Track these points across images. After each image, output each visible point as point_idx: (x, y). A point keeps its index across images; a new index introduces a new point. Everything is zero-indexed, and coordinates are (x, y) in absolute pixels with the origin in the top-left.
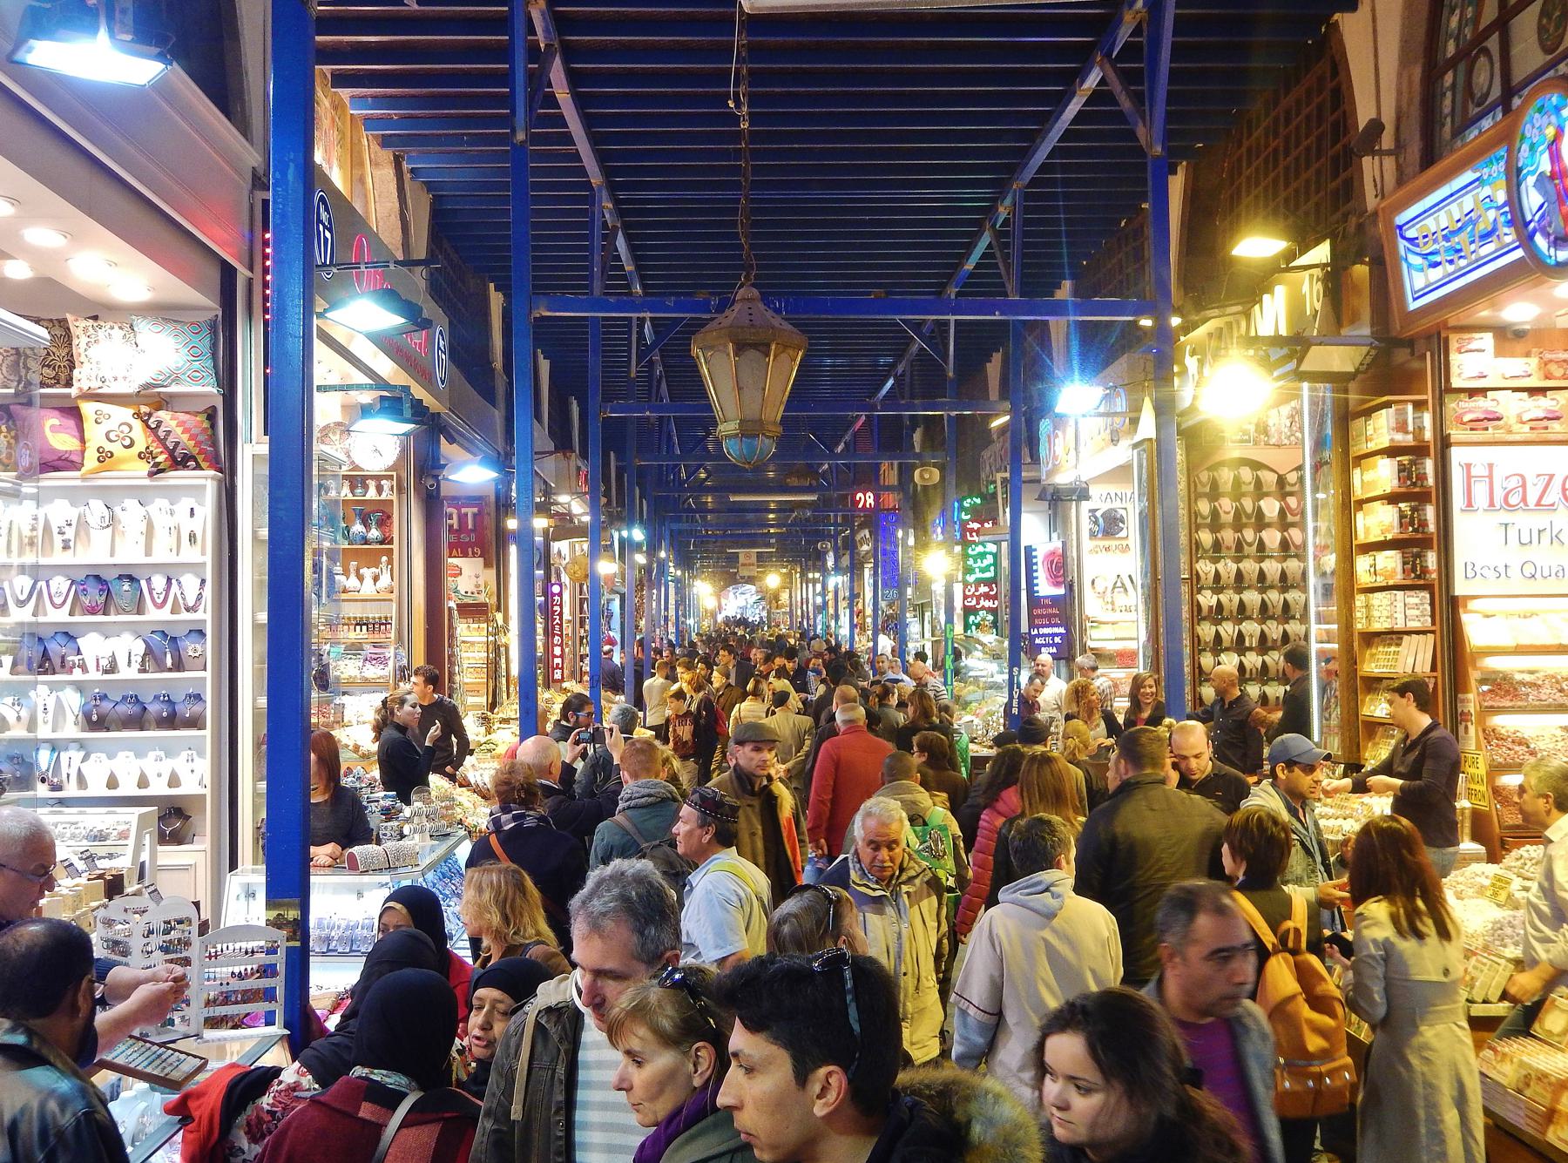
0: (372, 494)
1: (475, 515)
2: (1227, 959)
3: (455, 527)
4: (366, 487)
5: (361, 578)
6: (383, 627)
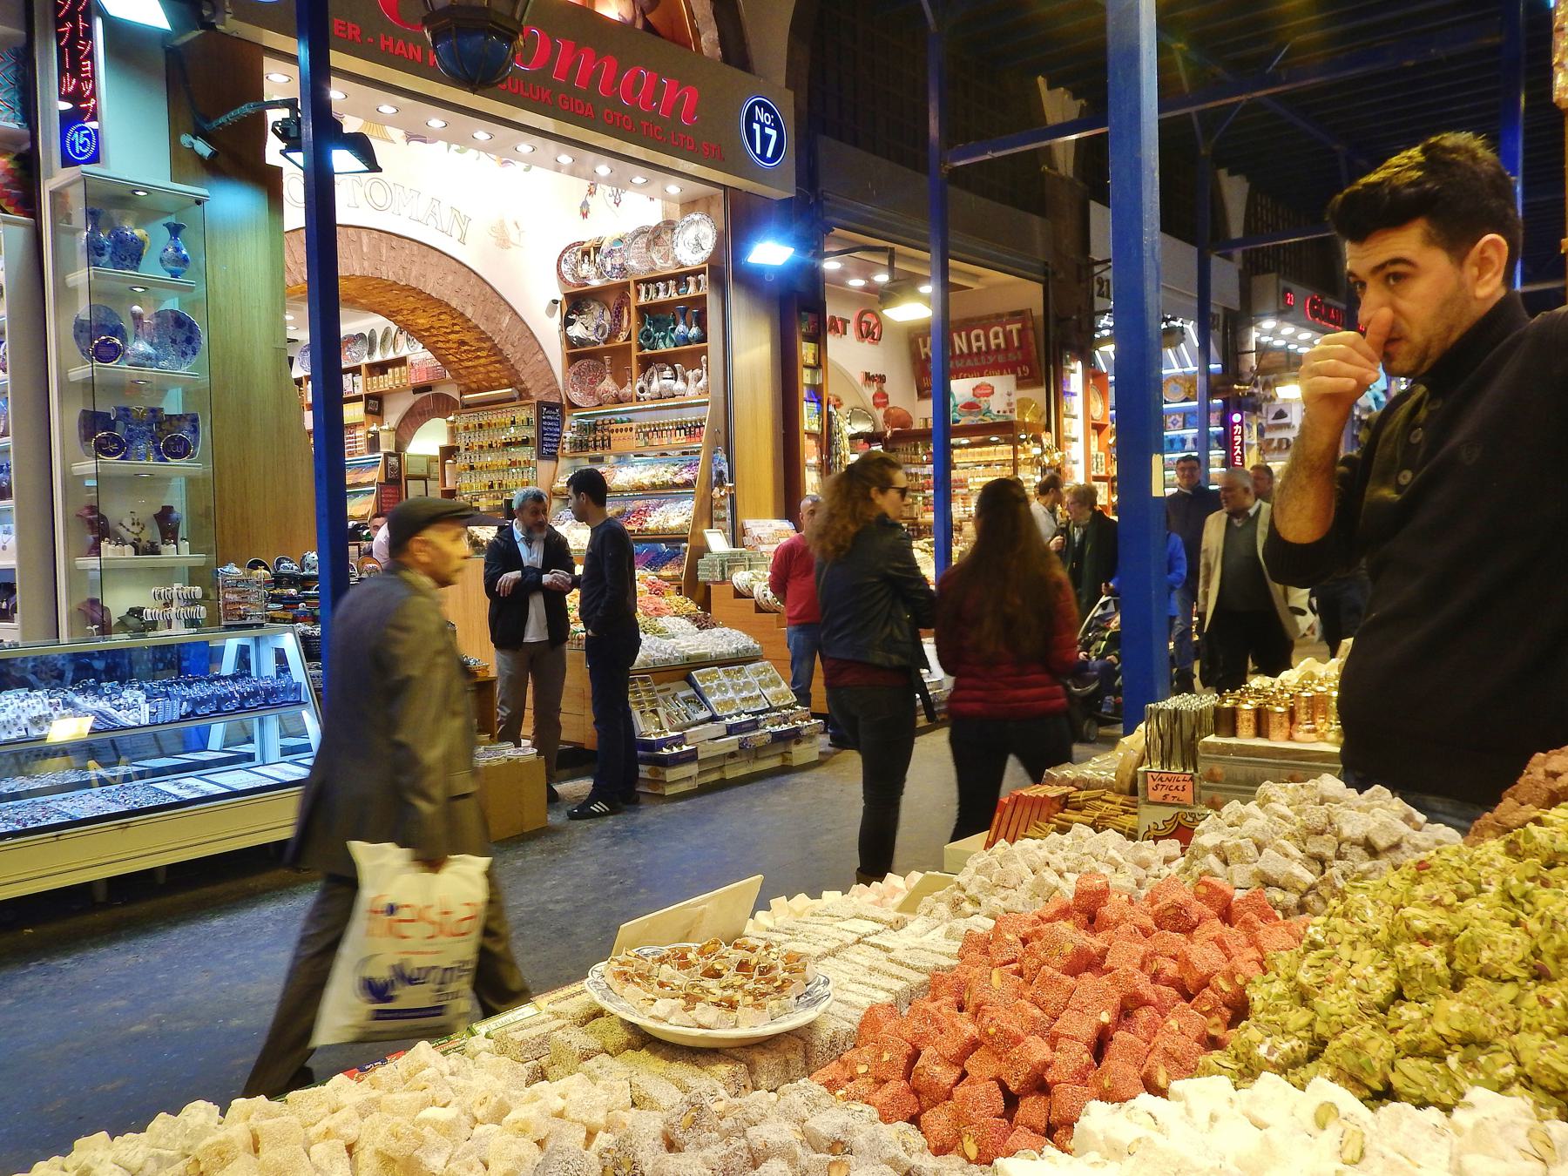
0: (692, 291)
1: (1019, 331)
2: (1268, 885)
3: (1003, 346)
4: (687, 284)
5: (686, 380)
6: (697, 430)
